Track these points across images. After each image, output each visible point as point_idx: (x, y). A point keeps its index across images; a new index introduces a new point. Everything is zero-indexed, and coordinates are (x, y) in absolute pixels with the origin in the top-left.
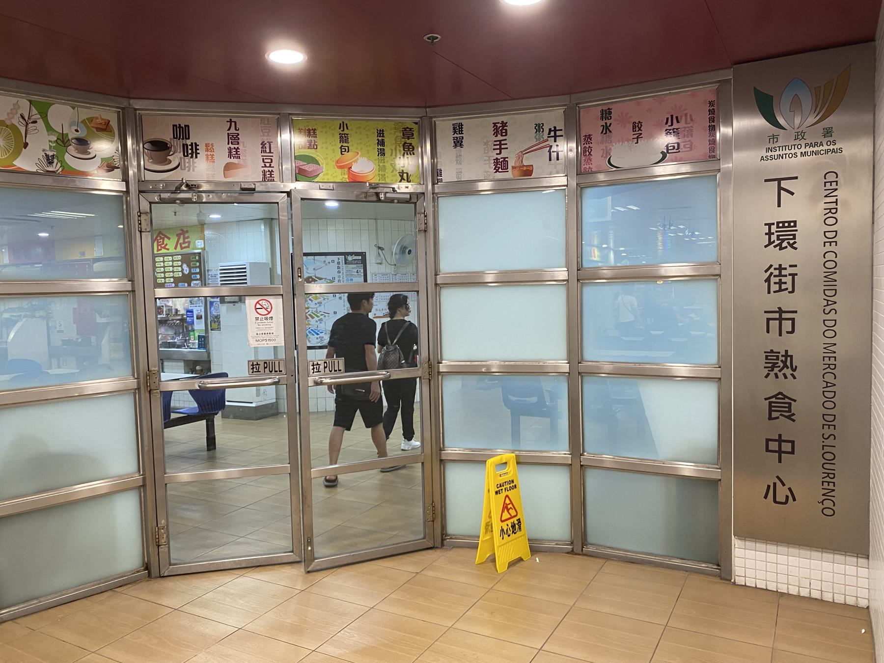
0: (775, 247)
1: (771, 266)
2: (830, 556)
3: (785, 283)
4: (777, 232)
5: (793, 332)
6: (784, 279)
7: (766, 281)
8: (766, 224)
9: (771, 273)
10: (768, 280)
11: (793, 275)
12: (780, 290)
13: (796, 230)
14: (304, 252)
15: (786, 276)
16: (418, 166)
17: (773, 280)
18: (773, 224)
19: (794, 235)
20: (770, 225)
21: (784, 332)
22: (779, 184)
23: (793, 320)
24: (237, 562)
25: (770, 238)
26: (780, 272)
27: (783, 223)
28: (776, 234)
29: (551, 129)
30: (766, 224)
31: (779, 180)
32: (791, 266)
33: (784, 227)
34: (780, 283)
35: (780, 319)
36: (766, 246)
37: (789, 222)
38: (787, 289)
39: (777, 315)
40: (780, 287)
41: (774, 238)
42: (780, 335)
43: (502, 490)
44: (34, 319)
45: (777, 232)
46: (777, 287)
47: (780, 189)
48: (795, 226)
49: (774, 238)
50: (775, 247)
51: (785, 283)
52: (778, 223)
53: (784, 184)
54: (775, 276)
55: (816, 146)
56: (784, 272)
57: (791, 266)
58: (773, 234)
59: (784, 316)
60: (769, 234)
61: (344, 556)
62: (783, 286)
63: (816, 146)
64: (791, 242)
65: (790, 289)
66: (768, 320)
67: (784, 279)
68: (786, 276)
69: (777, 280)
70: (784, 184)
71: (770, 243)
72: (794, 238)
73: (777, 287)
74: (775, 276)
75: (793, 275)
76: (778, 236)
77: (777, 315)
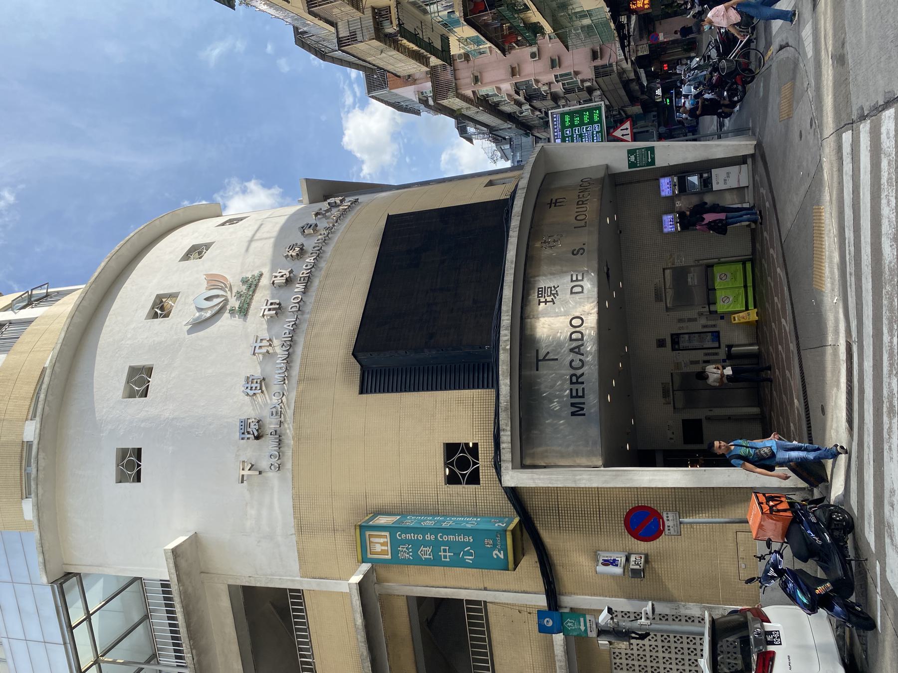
0: (555, 298)
18: (539, 300)
19: (548, 288)
36: (554, 303)
41: (549, 299)
49: (549, 299)
50: (555, 298)
55: (580, 380)
58: (546, 300)
63: (580, 380)
71: (553, 301)
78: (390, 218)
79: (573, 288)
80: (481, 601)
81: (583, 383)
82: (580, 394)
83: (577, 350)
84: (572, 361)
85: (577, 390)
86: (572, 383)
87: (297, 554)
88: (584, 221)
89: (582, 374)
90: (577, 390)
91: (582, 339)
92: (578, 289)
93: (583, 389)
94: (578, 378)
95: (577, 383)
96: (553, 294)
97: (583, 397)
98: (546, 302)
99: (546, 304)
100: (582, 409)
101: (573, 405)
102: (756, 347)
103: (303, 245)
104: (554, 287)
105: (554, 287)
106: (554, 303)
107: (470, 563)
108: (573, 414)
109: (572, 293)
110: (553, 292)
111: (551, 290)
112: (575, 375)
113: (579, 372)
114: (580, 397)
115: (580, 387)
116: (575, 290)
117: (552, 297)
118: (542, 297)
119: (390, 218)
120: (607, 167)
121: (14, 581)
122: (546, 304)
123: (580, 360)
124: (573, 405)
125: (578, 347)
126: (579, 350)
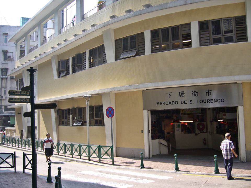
2: (72, 180)
5: (211, 95)
6: (195, 94)
10: (193, 94)
11: (197, 93)
12: (195, 96)
20: (180, 92)
23: (211, 92)
24: (183, 120)
29: (13, 77)
31: (169, 93)
35: (208, 92)
37: (183, 92)
39: (208, 92)
41: (180, 95)
42: (209, 95)
43: (13, 155)
44: (198, 135)
46: (194, 95)
47: (169, 95)
49: (180, 95)
53: (170, 94)
55: (164, 104)
59: (209, 92)
60: (180, 94)
63: (164, 104)
65: (197, 95)
66: (206, 93)
67: (195, 94)
69: (194, 94)
70: (170, 94)
71: (180, 96)
73: (194, 95)
75: (197, 93)
77: (208, 92)
79: (183, 101)
80: (190, 39)
81: (207, 102)
82: (161, 104)
84: (168, 102)
86: (163, 102)
87: (145, 145)
88: (199, 102)
92: (182, 103)
95: (163, 103)
96: (182, 96)
97: (185, 103)
100: (158, 105)
101: (159, 102)
103: (210, 121)
108: (157, 103)
109: (181, 101)
111: (183, 95)
112: (209, 101)
113: (165, 104)
115: (162, 104)
121: (29, 162)
124: (159, 102)
125: (171, 103)
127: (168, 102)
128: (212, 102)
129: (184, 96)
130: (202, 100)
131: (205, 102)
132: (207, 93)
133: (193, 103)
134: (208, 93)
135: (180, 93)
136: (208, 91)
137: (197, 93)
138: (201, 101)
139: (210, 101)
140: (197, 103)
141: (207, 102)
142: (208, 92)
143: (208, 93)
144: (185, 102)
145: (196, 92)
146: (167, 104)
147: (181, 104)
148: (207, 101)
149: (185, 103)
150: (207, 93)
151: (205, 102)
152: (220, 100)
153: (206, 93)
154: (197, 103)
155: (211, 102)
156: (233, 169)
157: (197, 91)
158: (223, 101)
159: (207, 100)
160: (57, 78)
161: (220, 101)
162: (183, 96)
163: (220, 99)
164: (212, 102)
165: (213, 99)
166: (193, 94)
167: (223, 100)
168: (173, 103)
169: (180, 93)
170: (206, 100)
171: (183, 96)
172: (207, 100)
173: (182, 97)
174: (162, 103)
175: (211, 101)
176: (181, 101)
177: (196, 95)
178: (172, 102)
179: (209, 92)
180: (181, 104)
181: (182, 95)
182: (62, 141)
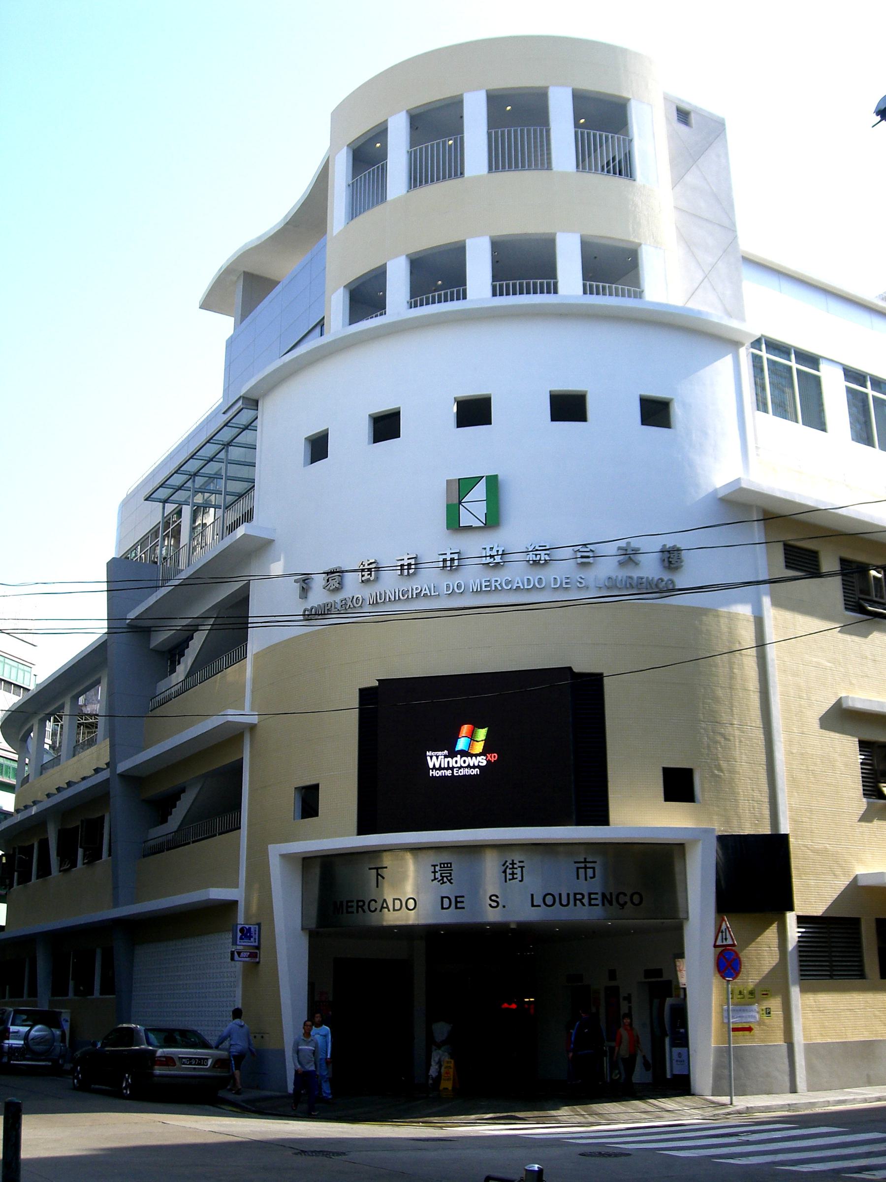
0: (439, 881)
1: (506, 861)
3: (516, 874)
4: (440, 870)
6: (515, 871)
7: (503, 872)
8: (432, 866)
9: (507, 866)
11: (522, 867)
12: (513, 878)
13: (452, 870)
14: (558, 234)
15: (516, 868)
16: (637, 551)
17: (509, 871)
18: (437, 865)
19: (450, 873)
20: (434, 866)
21: (588, 878)
22: (377, 871)
23: (593, 868)
25: (435, 876)
26: (513, 866)
27: (444, 864)
28: (439, 872)
30: (432, 866)
32: (520, 862)
33: (444, 867)
34: (513, 874)
35: (586, 868)
36: (432, 880)
37: (447, 864)
38: (516, 878)
39: (582, 865)
40: (513, 877)
41: (438, 875)
42: (586, 879)
45: (440, 870)
46: (511, 877)
48: (451, 867)
50: (439, 881)
51: (516, 874)
52: (441, 864)
54: (510, 869)
55: (578, 902)
56: (515, 866)
57: (520, 862)
58: (437, 872)
59: (588, 865)
61: (873, 534)
62: (515, 876)
63: (578, 902)
64: (449, 878)
66: (578, 868)
67: (515, 871)
68: (516, 868)
69: (510, 871)
71: (435, 879)
72: (450, 876)
73: (511, 877)
74: (510, 869)
76: (441, 874)
77: (582, 865)
78: (398, 435)
81: (357, 912)
83: (385, 905)
84: (376, 901)
85: (596, 899)
89: (364, 911)
90: (596, 899)
91: (394, 910)
93: (597, 905)
94: (580, 900)
95: (358, 906)
96: (442, 879)
97: (457, 908)
98: (435, 872)
99: (432, 872)
102: (16, 874)
104: (451, 879)
105: (451, 879)
106: (432, 880)
107: (48, 1065)
109: (442, 898)
110: (445, 879)
111: (446, 877)
112: (364, 904)
113: (366, 907)
114: (347, 910)
116: (446, 901)
117: (440, 878)
118: (441, 867)
119: (398, 435)
120: (687, 918)
122: (432, 872)
123: (376, 909)
125: (387, 907)
126: (385, 908)
127: (376, 901)
128: (593, 902)
129: (449, 881)
130: (553, 896)
131: (564, 902)
132: (582, 871)
133: (500, 906)
134: (583, 870)
135: (438, 868)
136: (585, 861)
137: (520, 869)
138: (549, 900)
139: (585, 901)
140: (533, 905)
141: (575, 905)
142: (586, 868)
143: (583, 870)
144: (457, 902)
145: (519, 864)
146: (373, 909)
147: (443, 908)
148: (575, 900)
149: (457, 908)
150: (582, 871)
151: (564, 902)
152: (627, 899)
153: (578, 868)
154: (533, 905)
155: (590, 904)
156: (26, 1116)
157: (522, 862)
158: (412, 908)
159: (575, 894)
160: (389, 120)
161: (626, 903)
162: (445, 879)
163: (625, 895)
164: (593, 902)
165: (596, 894)
166: (505, 872)
167: (636, 899)
168: (397, 906)
169: (438, 868)
170: (568, 895)
171: (445, 879)
172: (575, 894)
173: (444, 883)
174: (355, 904)
175: (590, 899)
176: (442, 898)
177: (519, 876)
178: (394, 900)
179: (588, 865)
180: (443, 908)
181: (443, 877)
182: (272, 563)
